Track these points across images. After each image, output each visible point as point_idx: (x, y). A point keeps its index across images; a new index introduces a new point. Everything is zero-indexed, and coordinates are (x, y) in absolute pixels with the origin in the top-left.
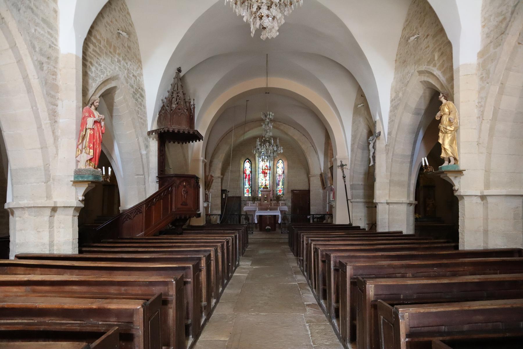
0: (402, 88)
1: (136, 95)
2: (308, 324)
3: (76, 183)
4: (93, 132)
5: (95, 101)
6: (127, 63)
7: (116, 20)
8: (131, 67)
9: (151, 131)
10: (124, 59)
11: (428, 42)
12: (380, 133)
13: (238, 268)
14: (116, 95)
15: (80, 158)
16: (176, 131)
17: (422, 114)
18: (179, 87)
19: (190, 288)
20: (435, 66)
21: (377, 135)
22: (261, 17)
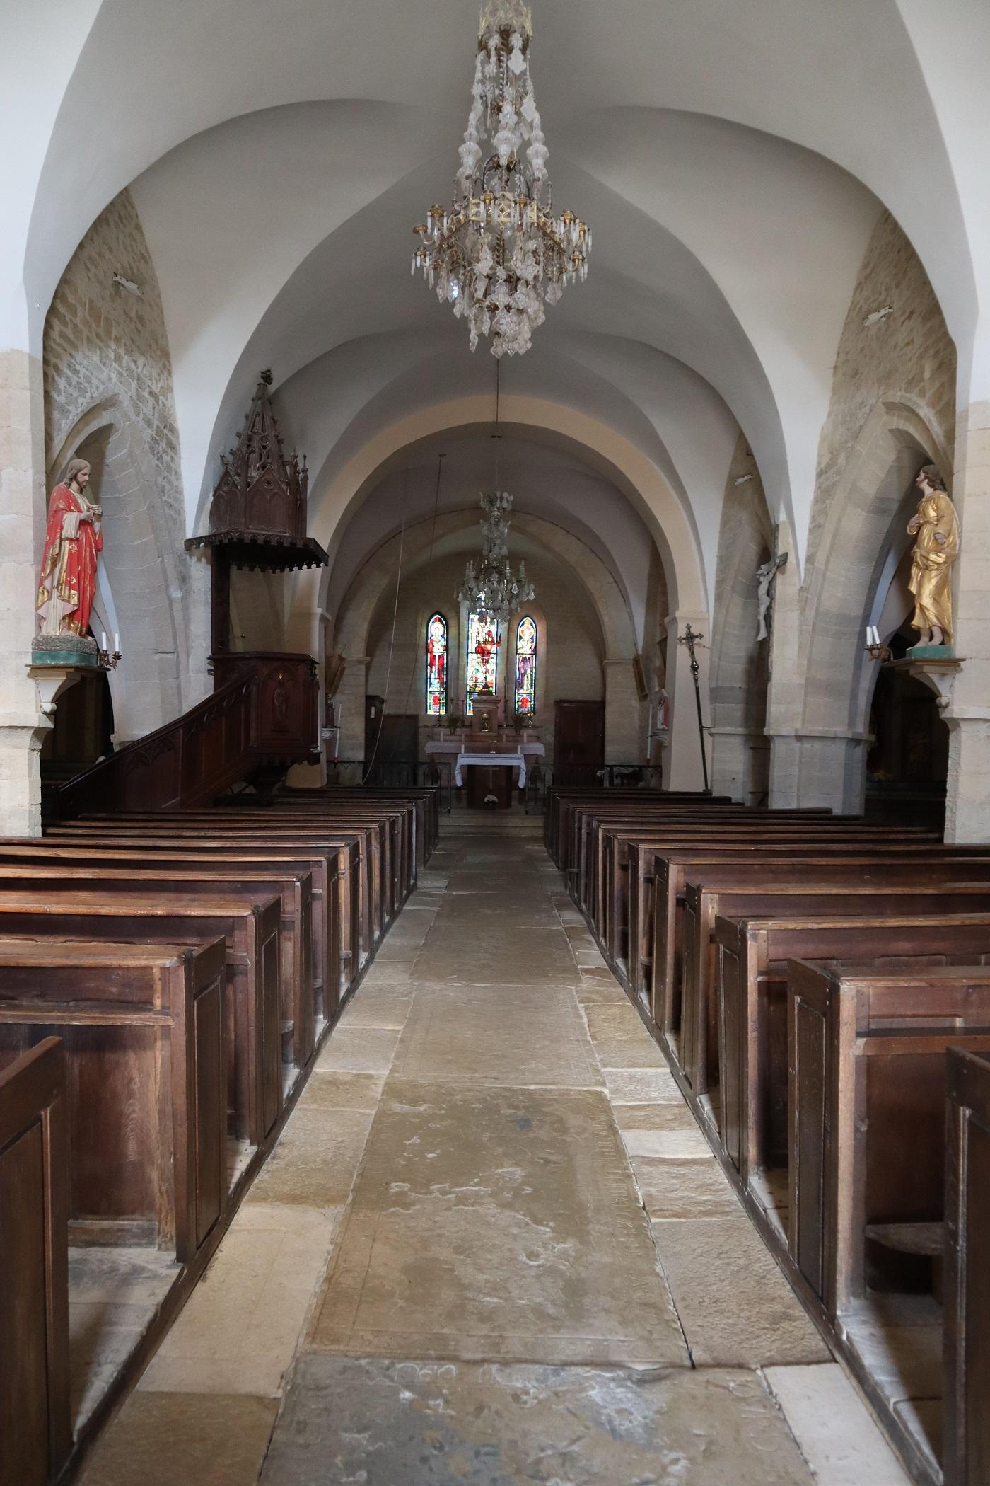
0: (846, 442)
1: (159, 445)
2: (583, 1005)
3: (37, 671)
4: (76, 548)
5: (80, 470)
6: (135, 362)
7: (111, 250)
8: (145, 372)
9: (196, 539)
10: (129, 352)
11: (911, 330)
12: (786, 556)
13: (414, 893)
14: (109, 445)
15: (48, 610)
16: (260, 542)
17: (894, 512)
18: (268, 422)
19: (246, 989)
20: (922, 393)
21: (778, 561)
22: (494, 308)
